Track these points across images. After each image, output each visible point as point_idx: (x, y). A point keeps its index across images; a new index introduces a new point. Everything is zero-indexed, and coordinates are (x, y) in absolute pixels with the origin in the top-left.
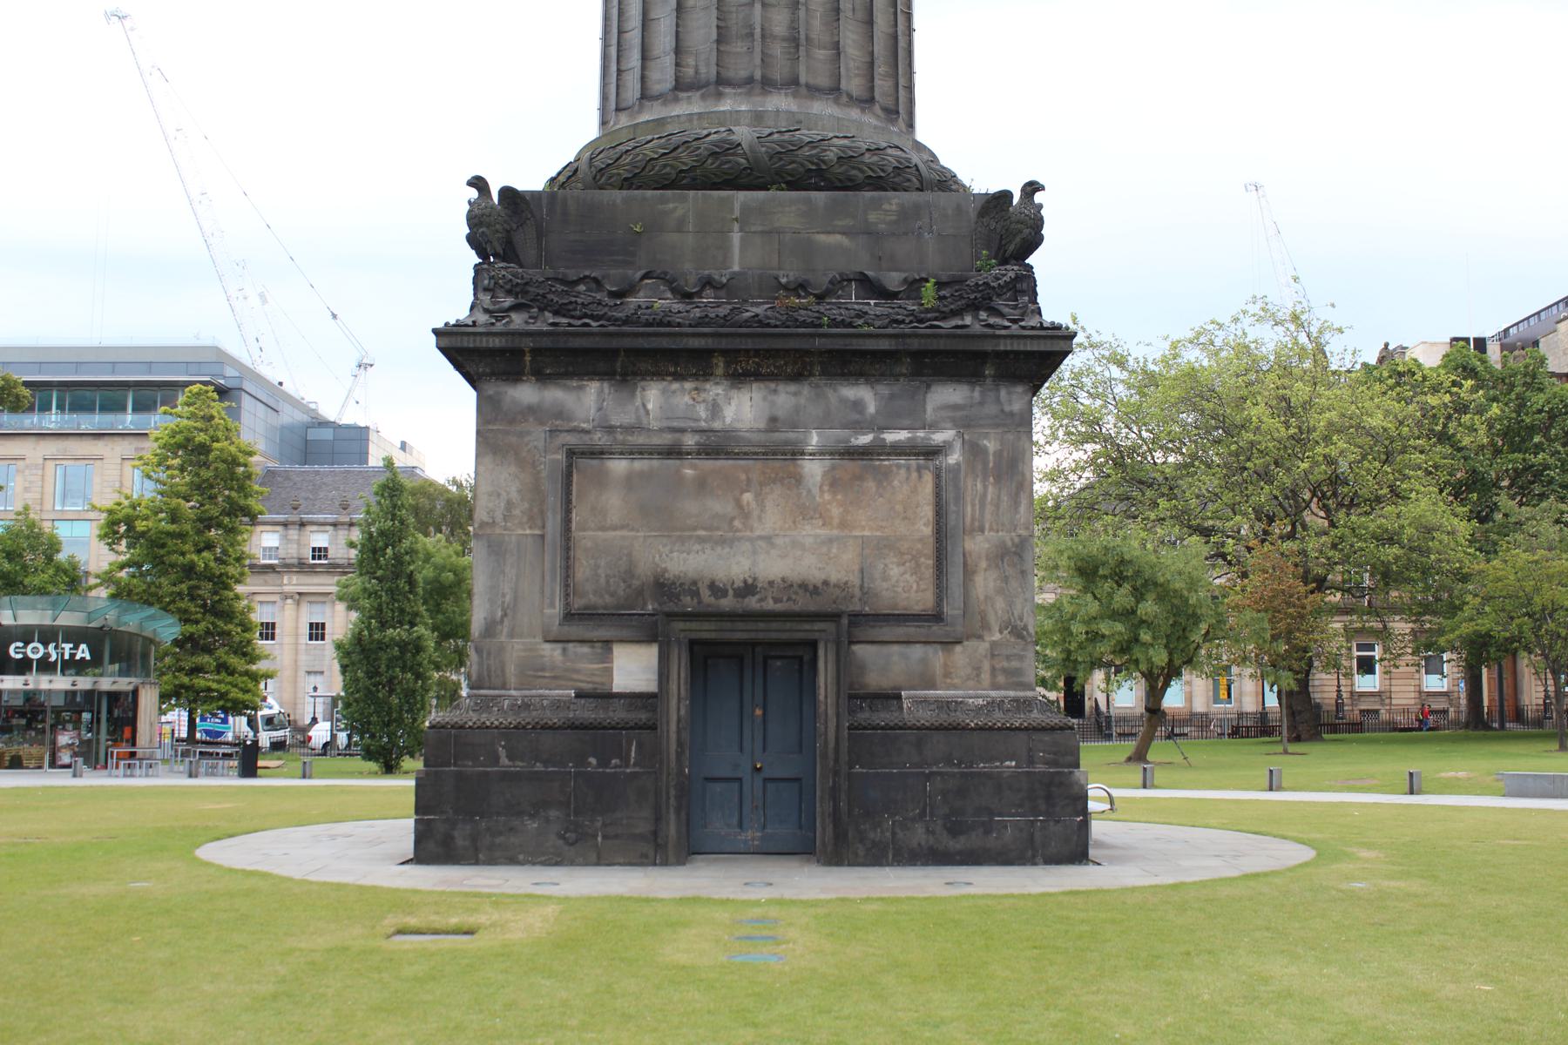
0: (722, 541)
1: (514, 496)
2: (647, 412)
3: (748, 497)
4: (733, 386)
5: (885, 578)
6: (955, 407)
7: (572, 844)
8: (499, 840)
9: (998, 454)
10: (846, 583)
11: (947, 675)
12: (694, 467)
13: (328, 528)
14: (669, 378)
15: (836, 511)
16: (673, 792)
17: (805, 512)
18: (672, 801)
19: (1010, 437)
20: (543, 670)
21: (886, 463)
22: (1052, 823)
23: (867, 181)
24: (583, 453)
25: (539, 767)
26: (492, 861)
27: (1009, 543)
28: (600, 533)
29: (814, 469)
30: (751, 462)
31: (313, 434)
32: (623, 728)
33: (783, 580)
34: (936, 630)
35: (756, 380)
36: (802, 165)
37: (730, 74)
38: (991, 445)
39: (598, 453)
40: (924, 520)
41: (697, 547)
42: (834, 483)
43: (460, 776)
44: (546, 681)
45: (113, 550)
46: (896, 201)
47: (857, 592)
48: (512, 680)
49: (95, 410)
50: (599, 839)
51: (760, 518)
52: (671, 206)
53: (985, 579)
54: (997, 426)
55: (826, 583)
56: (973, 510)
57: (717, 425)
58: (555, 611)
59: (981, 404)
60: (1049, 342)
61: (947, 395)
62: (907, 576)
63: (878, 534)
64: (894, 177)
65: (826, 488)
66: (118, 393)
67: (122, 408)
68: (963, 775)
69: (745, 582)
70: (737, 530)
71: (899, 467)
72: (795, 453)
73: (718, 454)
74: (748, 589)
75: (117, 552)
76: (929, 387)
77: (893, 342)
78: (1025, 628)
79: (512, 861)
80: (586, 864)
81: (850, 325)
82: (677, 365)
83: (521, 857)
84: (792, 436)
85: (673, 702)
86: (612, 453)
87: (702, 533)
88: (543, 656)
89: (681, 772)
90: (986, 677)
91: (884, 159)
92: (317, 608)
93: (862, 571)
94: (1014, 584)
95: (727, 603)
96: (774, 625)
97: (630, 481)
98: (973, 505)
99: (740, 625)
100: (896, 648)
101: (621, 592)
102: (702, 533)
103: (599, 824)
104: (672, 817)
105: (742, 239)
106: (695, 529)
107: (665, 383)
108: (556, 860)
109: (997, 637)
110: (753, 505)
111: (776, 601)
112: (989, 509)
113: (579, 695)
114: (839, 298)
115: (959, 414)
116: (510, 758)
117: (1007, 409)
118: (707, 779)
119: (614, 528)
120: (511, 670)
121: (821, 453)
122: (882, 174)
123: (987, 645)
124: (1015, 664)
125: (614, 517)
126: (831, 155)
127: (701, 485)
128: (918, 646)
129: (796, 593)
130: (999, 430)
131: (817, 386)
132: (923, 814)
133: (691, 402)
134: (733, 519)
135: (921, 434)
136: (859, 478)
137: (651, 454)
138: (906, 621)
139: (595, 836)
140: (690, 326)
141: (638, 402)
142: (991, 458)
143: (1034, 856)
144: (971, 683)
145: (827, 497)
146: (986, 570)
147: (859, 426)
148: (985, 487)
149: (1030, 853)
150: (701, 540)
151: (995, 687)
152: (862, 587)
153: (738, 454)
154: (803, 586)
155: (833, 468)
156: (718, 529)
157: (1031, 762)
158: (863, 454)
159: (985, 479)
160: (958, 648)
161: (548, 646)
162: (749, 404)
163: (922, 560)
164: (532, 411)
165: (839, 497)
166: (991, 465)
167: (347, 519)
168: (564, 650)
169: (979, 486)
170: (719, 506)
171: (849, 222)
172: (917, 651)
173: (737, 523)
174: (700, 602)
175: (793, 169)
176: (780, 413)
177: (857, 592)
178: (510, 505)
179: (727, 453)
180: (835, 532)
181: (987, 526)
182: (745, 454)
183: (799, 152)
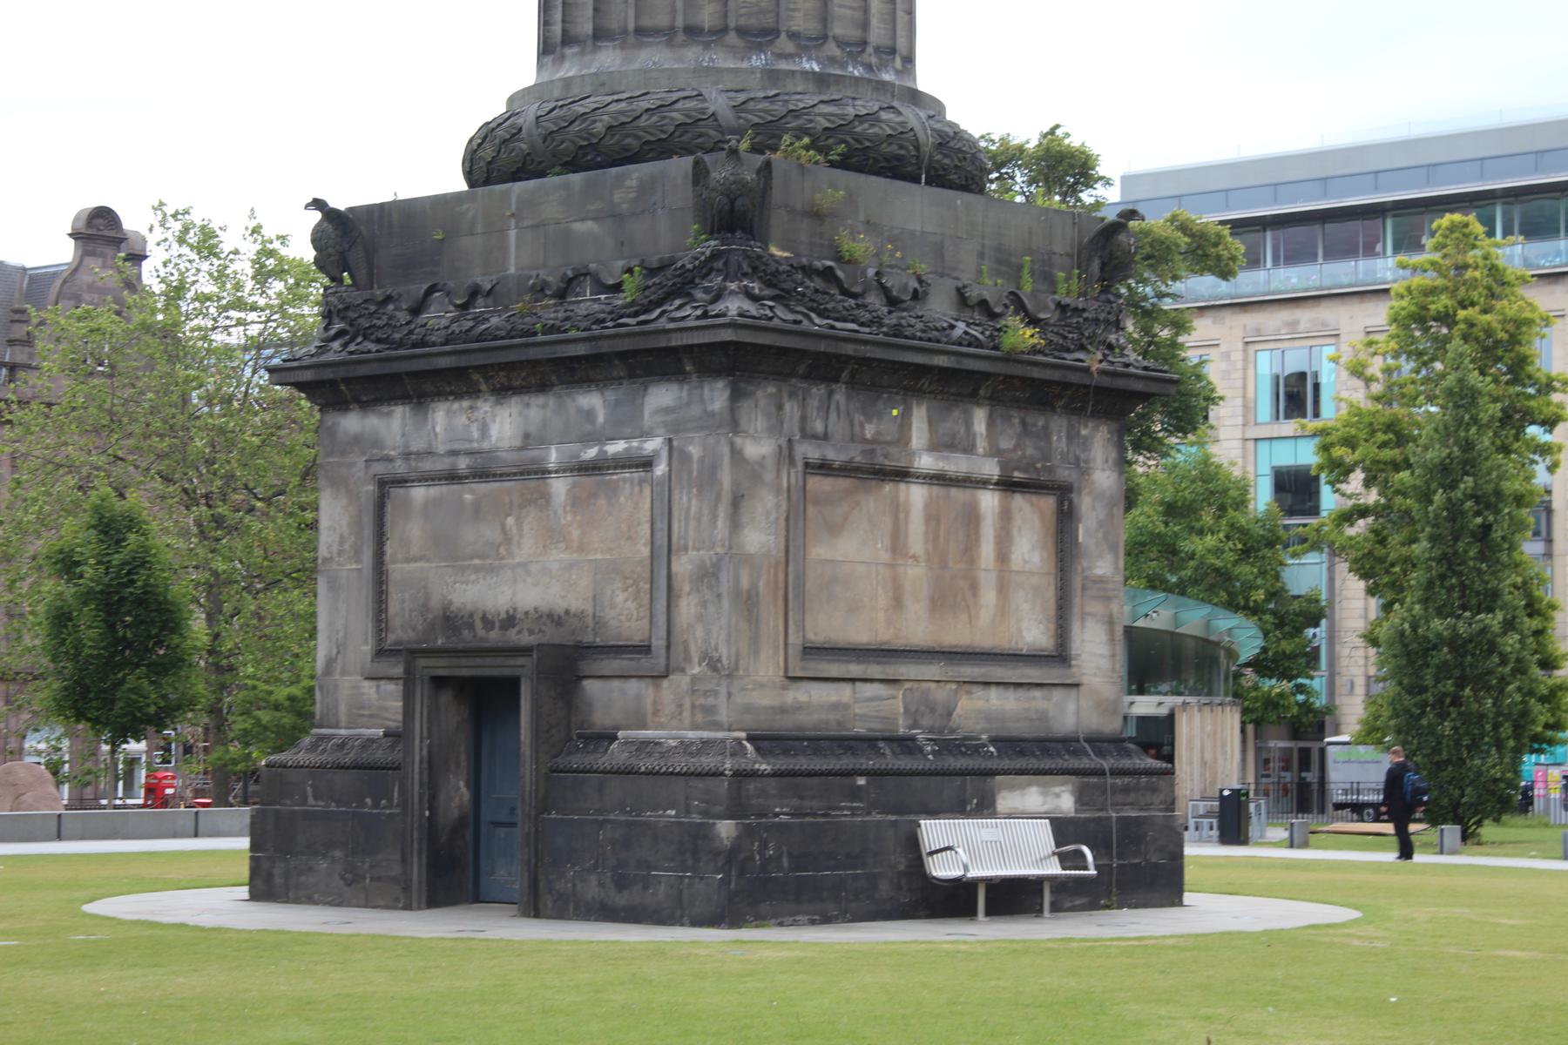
0: (491, 570)
1: (345, 530)
2: (436, 435)
3: (510, 521)
4: (498, 403)
5: (613, 606)
7: (349, 885)
8: (303, 878)
9: (702, 460)
10: (582, 612)
11: (656, 713)
12: (472, 492)
14: (451, 398)
15: (576, 533)
16: (416, 835)
18: (416, 845)
19: (711, 440)
20: (362, 708)
21: (615, 477)
22: (697, 880)
23: (646, 147)
24: (393, 482)
25: (333, 808)
26: (297, 901)
27: (708, 564)
28: (405, 565)
29: (559, 487)
30: (512, 483)
32: (390, 769)
33: (536, 609)
34: (644, 662)
35: (514, 394)
36: (573, 142)
37: (613, 24)
38: (694, 451)
39: (402, 482)
40: (643, 541)
41: (473, 577)
43: (277, 812)
44: (364, 719)
45: (1337, 491)
46: (635, 176)
47: (590, 621)
48: (343, 718)
49: (1558, 231)
50: (368, 881)
51: (519, 544)
52: (465, 206)
53: (688, 605)
54: (700, 428)
55: (567, 612)
56: (680, 527)
57: (486, 445)
58: (367, 649)
59: (688, 404)
60: (712, 332)
61: (662, 396)
62: (629, 602)
63: (608, 557)
64: (680, 136)
65: (568, 508)
66: (1534, 203)
68: (629, 824)
69: (507, 612)
70: (503, 558)
71: (624, 480)
72: (541, 472)
73: (487, 476)
74: (510, 621)
75: (1343, 495)
76: (646, 389)
77: (588, 345)
78: (719, 660)
79: (310, 901)
80: (359, 906)
81: (559, 330)
82: (449, 384)
83: (316, 896)
84: (536, 453)
85: (417, 742)
86: (413, 481)
87: (477, 561)
88: (363, 694)
89: (422, 814)
90: (686, 714)
91: (664, 117)
93: (594, 597)
94: (711, 609)
95: (494, 636)
96: (488, 661)
97: (431, 506)
98: (680, 521)
99: (464, 661)
100: (616, 683)
101: (420, 627)
102: (477, 561)
103: (367, 865)
104: (415, 860)
105: (518, 235)
106: (472, 558)
107: (448, 403)
108: (338, 902)
109: (696, 670)
110: (514, 530)
111: (531, 632)
112: (692, 524)
113: (386, 735)
114: (577, 296)
115: (670, 417)
116: (316, 797)
117: (710, 408)
118: (492, 823)
119: (416, 560)
120: (343, 708)
121: (563, 470)
122: (664, 136)
123: (687, 679)
124: (711, 701)
126: (599, 127)
128: (633, 680)
129: (545, 624)
130: (702, 434)
131: (560, 397)
132: (596, 866)
133: (467, 422)
134: (499, 546)
135: (635, 444)
136: (593, 495)
137: (440, 479)
138: (623, 652)
139: (364, 878)
140: (442, 344)
141: (429, 427)
142: (695, 466)
143: (682, 916)
144: (674, 722)
145: (569, 517)
146: (689, 594)
147: (588, 439)
148: (689, 500)
149: (678, 913)
150: (477, 569)
151: (695, 727)
152: (594, 616)
153: (501, 475)
154: (550, 616)
155: (574, 486)
156: (488, 557)
157: (688, 812)
158: (594, 469)
159: (689, 492)
160: (665, 683)
161: (367, 684)
162: (509, 420)
163: (641, 584)
164: (357, 440)
165: (578, 518)
166: (695, 474)
168: (378, 687)
169: (685, 499)
170: (490, 532)
171: (597, 205)
172: (633, 686)
173: (502, 550)
174: (475, 636)
175: (565, 149)
176: (532, 429)
177: (590, 621)
178: (342, 537)
179: (495, 475)
180: (575, 556)
181: (691, 544)
182: (508, 475)
183: (570, 128)
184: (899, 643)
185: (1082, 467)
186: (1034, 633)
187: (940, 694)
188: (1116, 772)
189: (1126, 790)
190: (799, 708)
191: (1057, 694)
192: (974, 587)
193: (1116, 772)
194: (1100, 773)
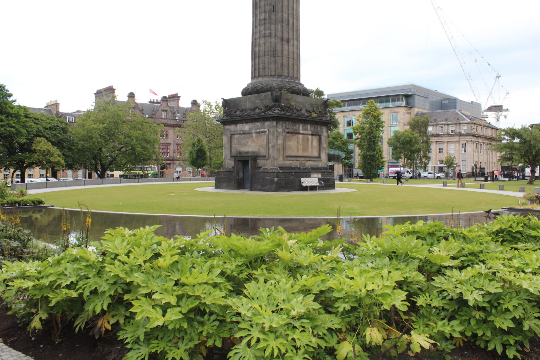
6: (268, 125)
13: (454, 125)
15: (256, 141)
17: (253, 141)
29: (254, 135)
31: (443, 102)
34: (265, 158)
37: (261, 74)
38: (272, 130)
39: (234, 135)
42: (256, 137)
61: (267, 123)
67: (389, 101)
74: (248, 153)
79: (223, 189)
92: (441, 145)
95: (246, 155)
108: (226, 189)
125: (235, 143)
126: (259, 88)
127: (243, 138)
147: (258, 129)
164: (228, 129)
167: (436, 124)
170: (245, 141)
172: (264, 161)
184: (298, 155)
185: (322, 133)
186: (316, 154)
187: (304, 162)
188: (326, 172)
189: (328, 174)
190: (285, 164)
191: (319, 162)
192: (308, 148)
193: (326, 172)
194: (324, 172)
